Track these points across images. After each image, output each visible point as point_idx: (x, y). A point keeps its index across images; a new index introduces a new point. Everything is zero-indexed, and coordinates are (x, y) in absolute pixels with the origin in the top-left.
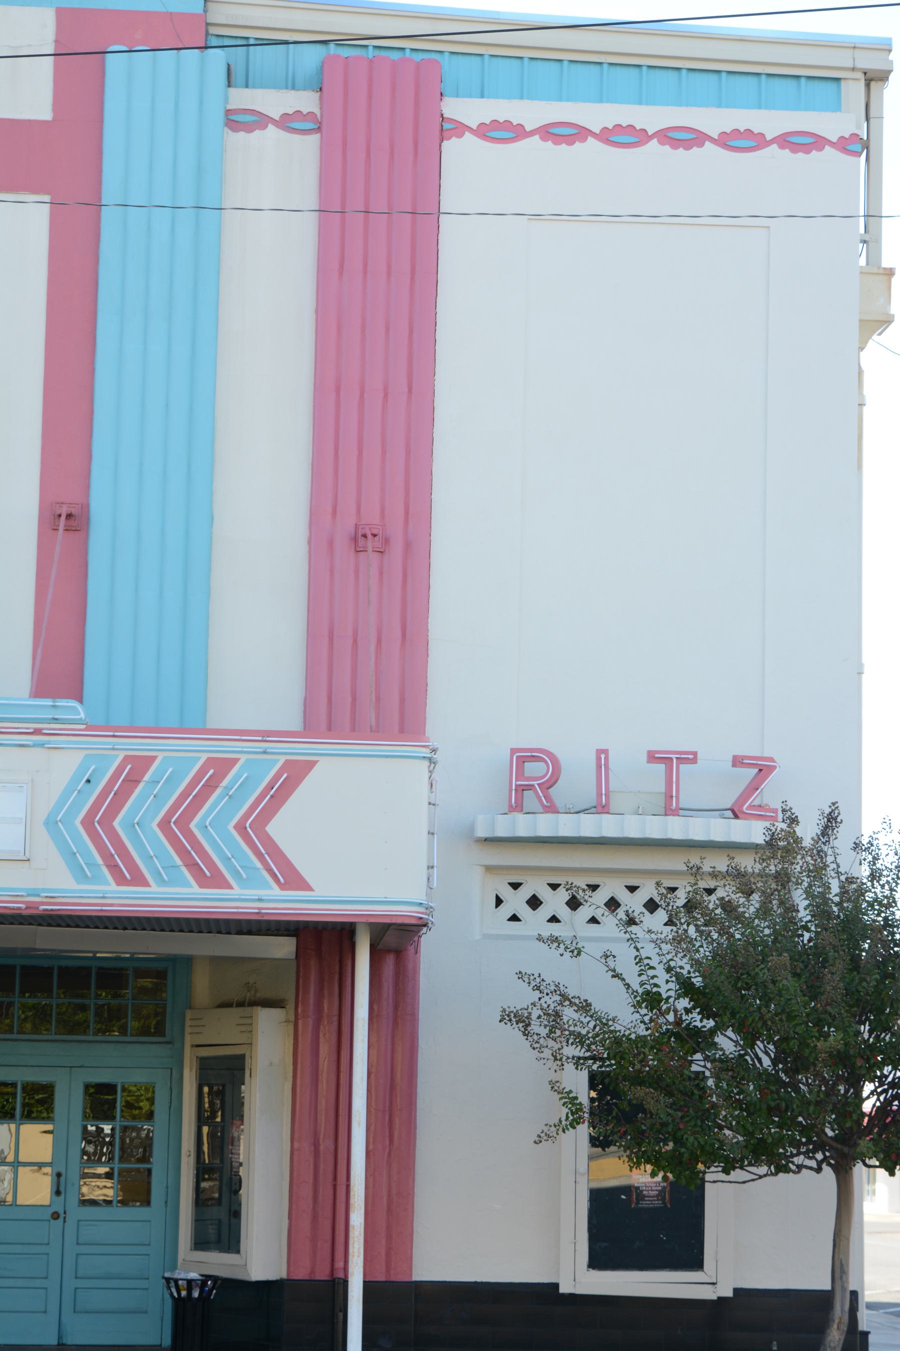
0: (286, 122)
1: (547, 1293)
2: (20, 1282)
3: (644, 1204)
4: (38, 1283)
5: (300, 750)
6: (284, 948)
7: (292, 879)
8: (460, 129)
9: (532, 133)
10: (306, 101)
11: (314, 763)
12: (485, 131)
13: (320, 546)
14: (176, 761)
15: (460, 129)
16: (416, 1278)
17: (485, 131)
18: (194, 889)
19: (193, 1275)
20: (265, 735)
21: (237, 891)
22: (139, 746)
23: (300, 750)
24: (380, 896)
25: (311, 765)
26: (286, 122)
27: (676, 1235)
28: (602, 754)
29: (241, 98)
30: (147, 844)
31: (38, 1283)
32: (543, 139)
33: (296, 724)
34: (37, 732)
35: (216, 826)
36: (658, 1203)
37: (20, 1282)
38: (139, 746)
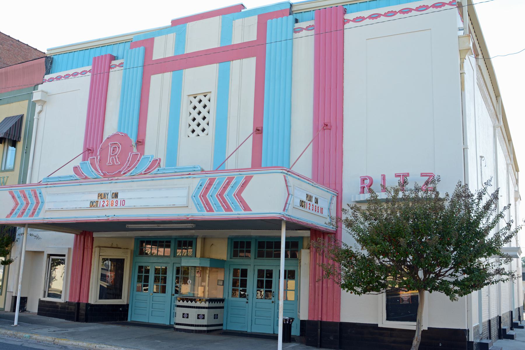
0: (307, 29)
1: (375, 327)
2: (265, 318)
3: (404, 303)
4: (269, 318)
5: (249, 173)
6: (307, 233)
7: (246, 208)
8: (349, 21)
9: (367, 18)
10: (312, 23)
11: (252, 176)
12: (354, 20)
13: (316, 129)
14: (221, 178)
15: (349, 21)
16: (341, 321)
17: (354, 20)
18: (224, 212)
19: (287, 318)
20: (240, 170)
21: (234, 212)
22: (212, 176)
23: (249, 173)
24: (268, 212)
25: (252, 177)
26: (307, 29)
27: (409, 310)
28: (384, 177)
29: (297, 25)
30: (214, 201)
31: (269, 318)
32: (369, 19)
33: (250, 167)
34: (190, 174)
35: (229, 196)
36: (408, 302)
37: (265, 318)
38: (212, 176)
